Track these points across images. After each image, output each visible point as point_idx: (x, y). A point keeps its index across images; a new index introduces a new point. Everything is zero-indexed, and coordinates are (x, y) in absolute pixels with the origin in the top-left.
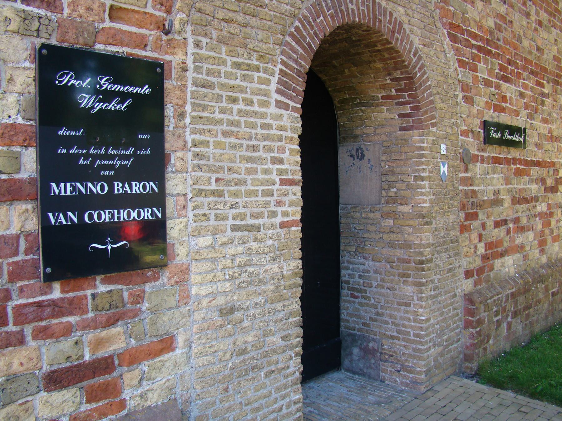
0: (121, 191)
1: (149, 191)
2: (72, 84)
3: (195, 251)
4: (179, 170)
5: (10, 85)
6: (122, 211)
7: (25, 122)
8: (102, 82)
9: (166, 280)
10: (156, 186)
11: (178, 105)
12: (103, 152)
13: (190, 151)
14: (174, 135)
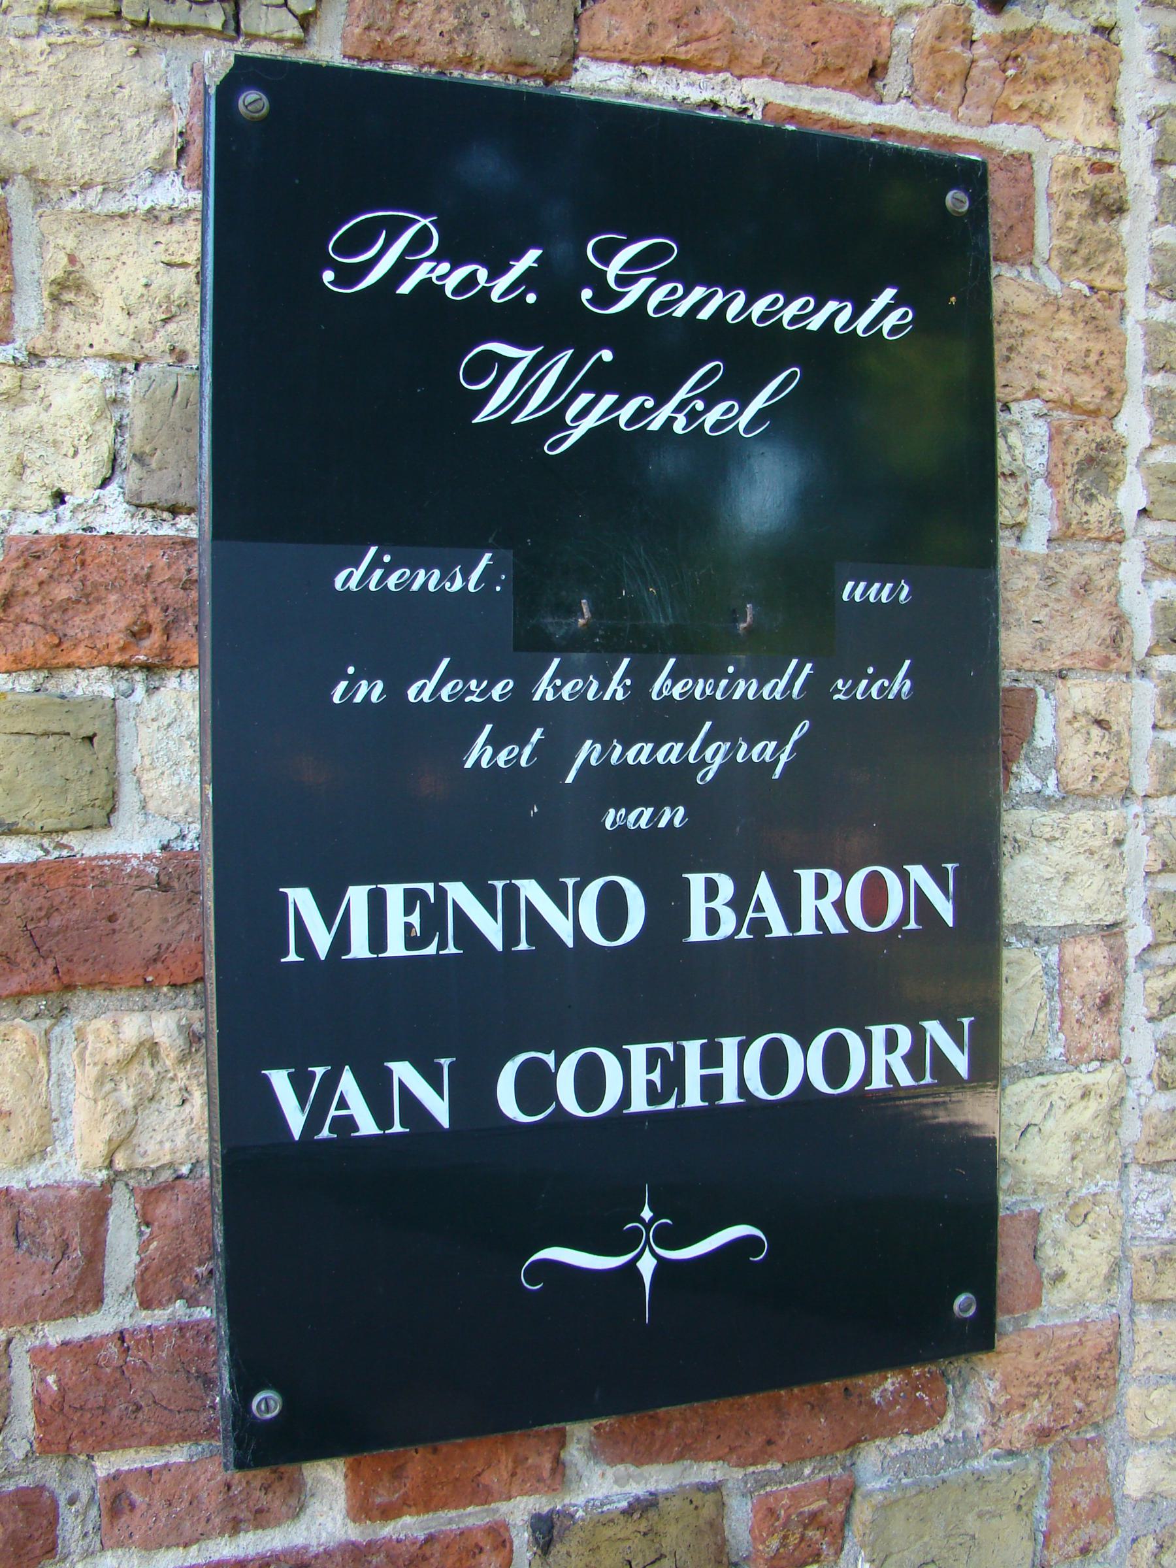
0: (727, 926)
1: (904, 917)
2: (426, 284)
3: (1156, 1250)
4: (1083, 785)
5: (66, 316)
6: (730, 1045)
7: (145, 526)
8: (613, 270)
9: (977, 1421)
10: (944, 888)
11: (1072, 407)
12: (616, 690)
13: (1143, 673)
14: (1050, 579)
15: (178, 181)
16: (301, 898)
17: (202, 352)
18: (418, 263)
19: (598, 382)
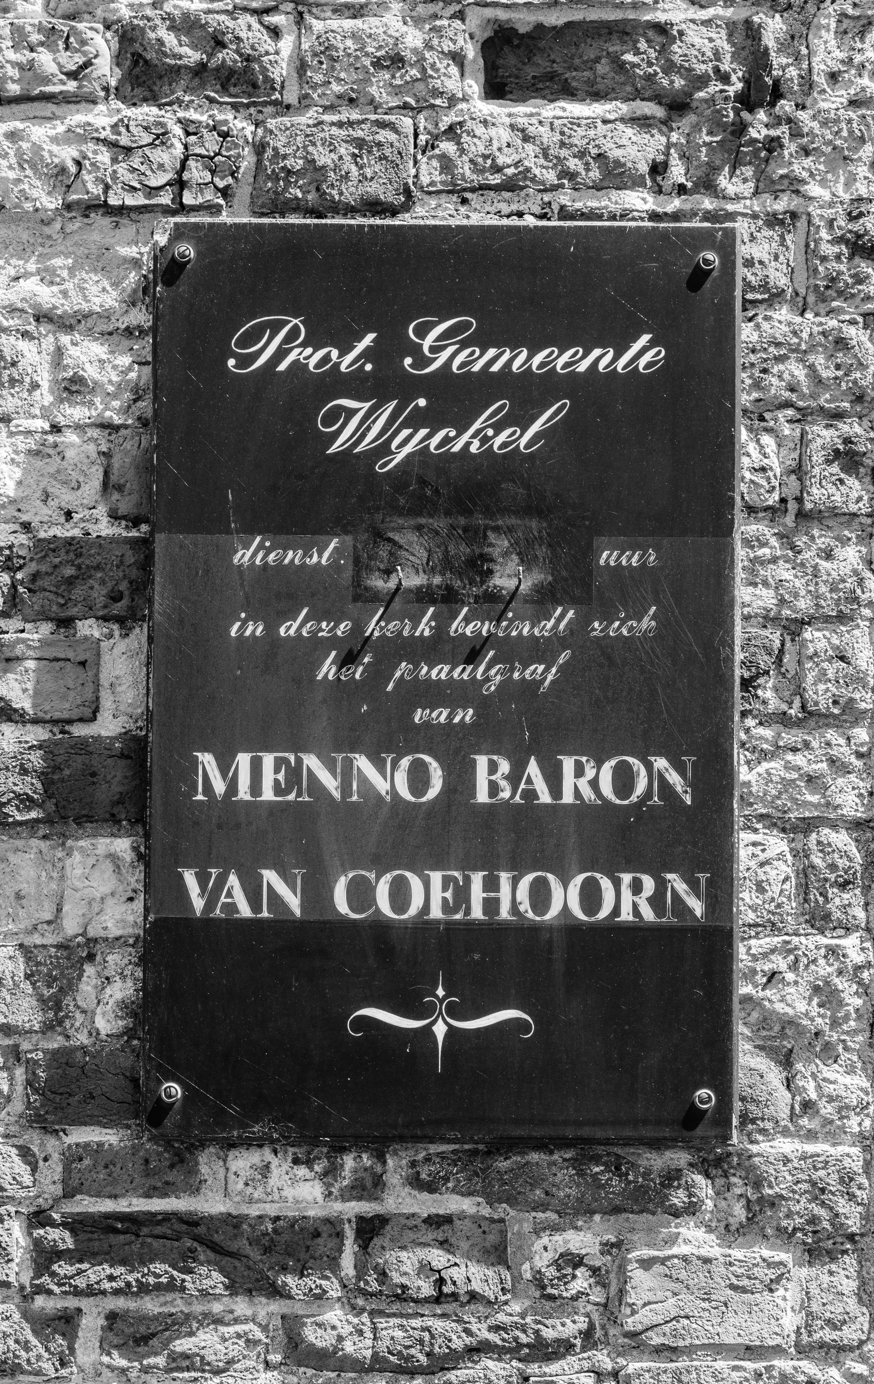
2: (296, 362)
6: (505, 878)
15: (144, 308)
16: (207, 760)
17: (148, 683)
18: (292, 349)
19: (415, 421)
